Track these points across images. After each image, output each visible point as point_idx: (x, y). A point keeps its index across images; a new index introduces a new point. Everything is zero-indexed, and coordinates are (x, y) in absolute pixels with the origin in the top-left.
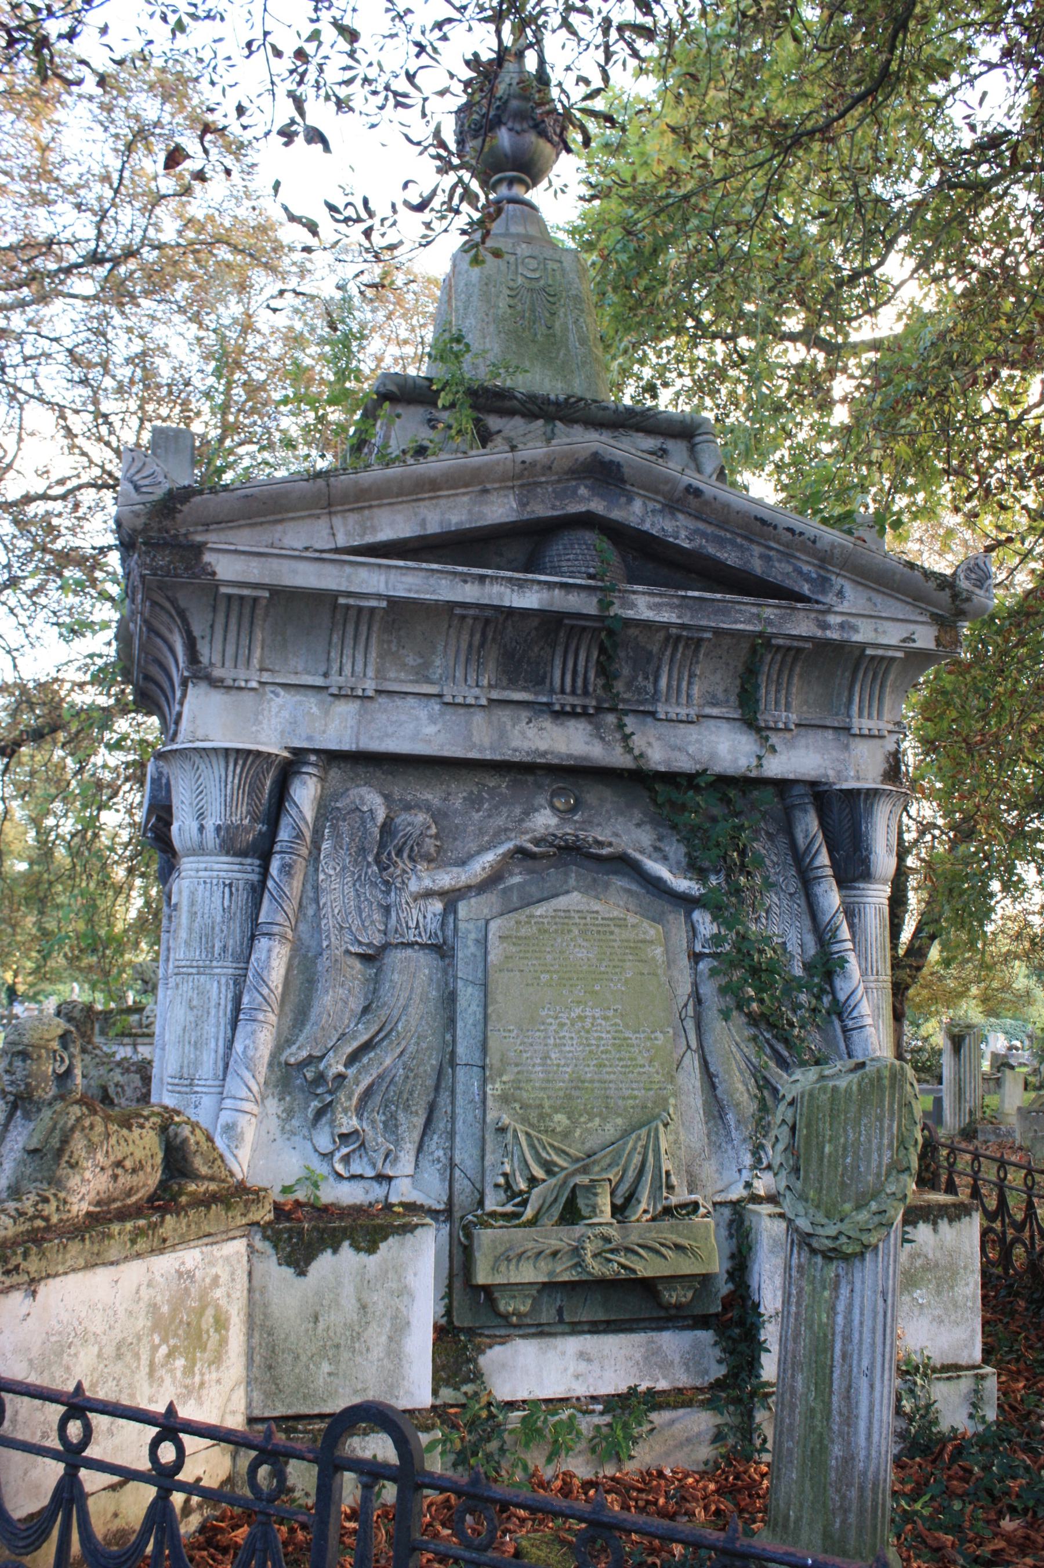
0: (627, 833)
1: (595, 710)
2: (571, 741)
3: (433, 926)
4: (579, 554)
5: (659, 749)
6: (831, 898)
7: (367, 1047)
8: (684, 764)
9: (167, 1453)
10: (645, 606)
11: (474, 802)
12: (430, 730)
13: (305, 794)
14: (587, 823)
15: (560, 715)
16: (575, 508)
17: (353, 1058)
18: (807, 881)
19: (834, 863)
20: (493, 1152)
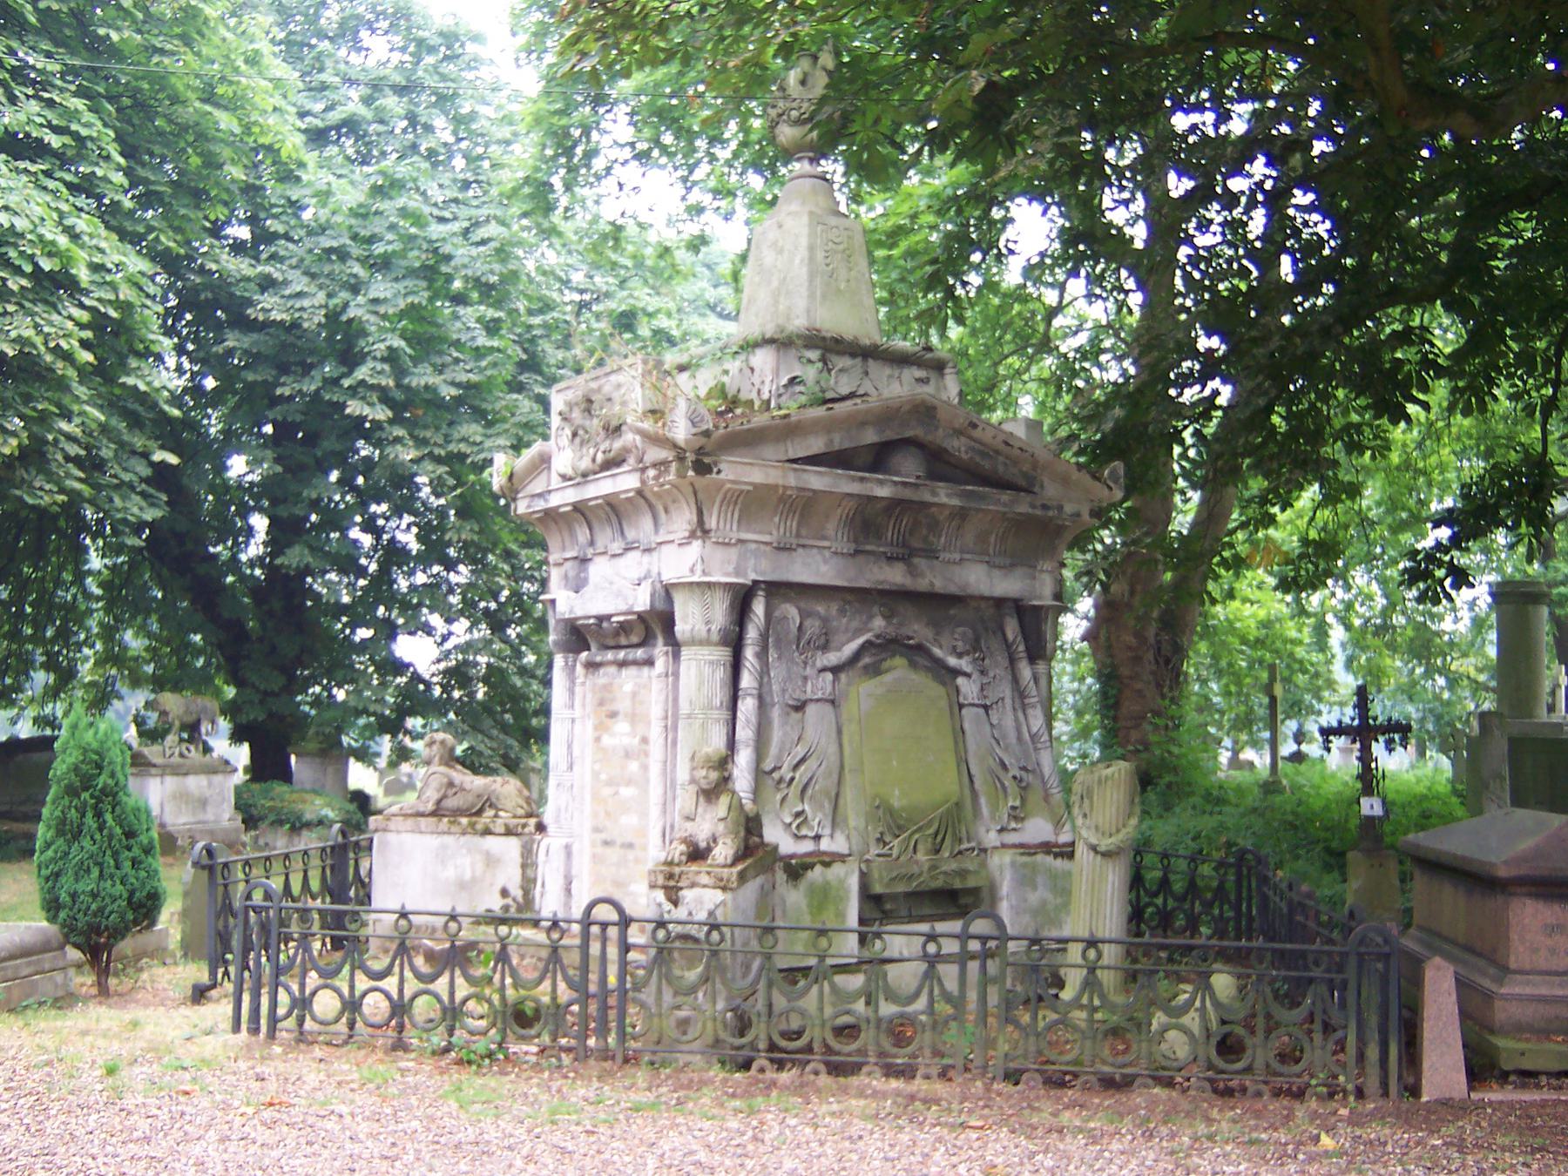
0: (918, 630)
1: (904, 555)
2: (895, 576)
3: (829, 689)
4: (909, 466)
5: (933, 578)
6: (1026, 672)
7: (803, 760)
8: (952, 589)
9: (1092, 954)
10: (944, 496)
11: (842, 612)
12: (824, 568)
13: (759, 607)
14: (901, 625)
15: (891, 559)
16: (909, 434)
17: (796, 767)
18: (1012, 661)
19: (1028, 650)
20: (182, 797)
